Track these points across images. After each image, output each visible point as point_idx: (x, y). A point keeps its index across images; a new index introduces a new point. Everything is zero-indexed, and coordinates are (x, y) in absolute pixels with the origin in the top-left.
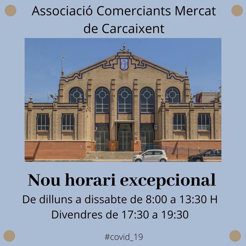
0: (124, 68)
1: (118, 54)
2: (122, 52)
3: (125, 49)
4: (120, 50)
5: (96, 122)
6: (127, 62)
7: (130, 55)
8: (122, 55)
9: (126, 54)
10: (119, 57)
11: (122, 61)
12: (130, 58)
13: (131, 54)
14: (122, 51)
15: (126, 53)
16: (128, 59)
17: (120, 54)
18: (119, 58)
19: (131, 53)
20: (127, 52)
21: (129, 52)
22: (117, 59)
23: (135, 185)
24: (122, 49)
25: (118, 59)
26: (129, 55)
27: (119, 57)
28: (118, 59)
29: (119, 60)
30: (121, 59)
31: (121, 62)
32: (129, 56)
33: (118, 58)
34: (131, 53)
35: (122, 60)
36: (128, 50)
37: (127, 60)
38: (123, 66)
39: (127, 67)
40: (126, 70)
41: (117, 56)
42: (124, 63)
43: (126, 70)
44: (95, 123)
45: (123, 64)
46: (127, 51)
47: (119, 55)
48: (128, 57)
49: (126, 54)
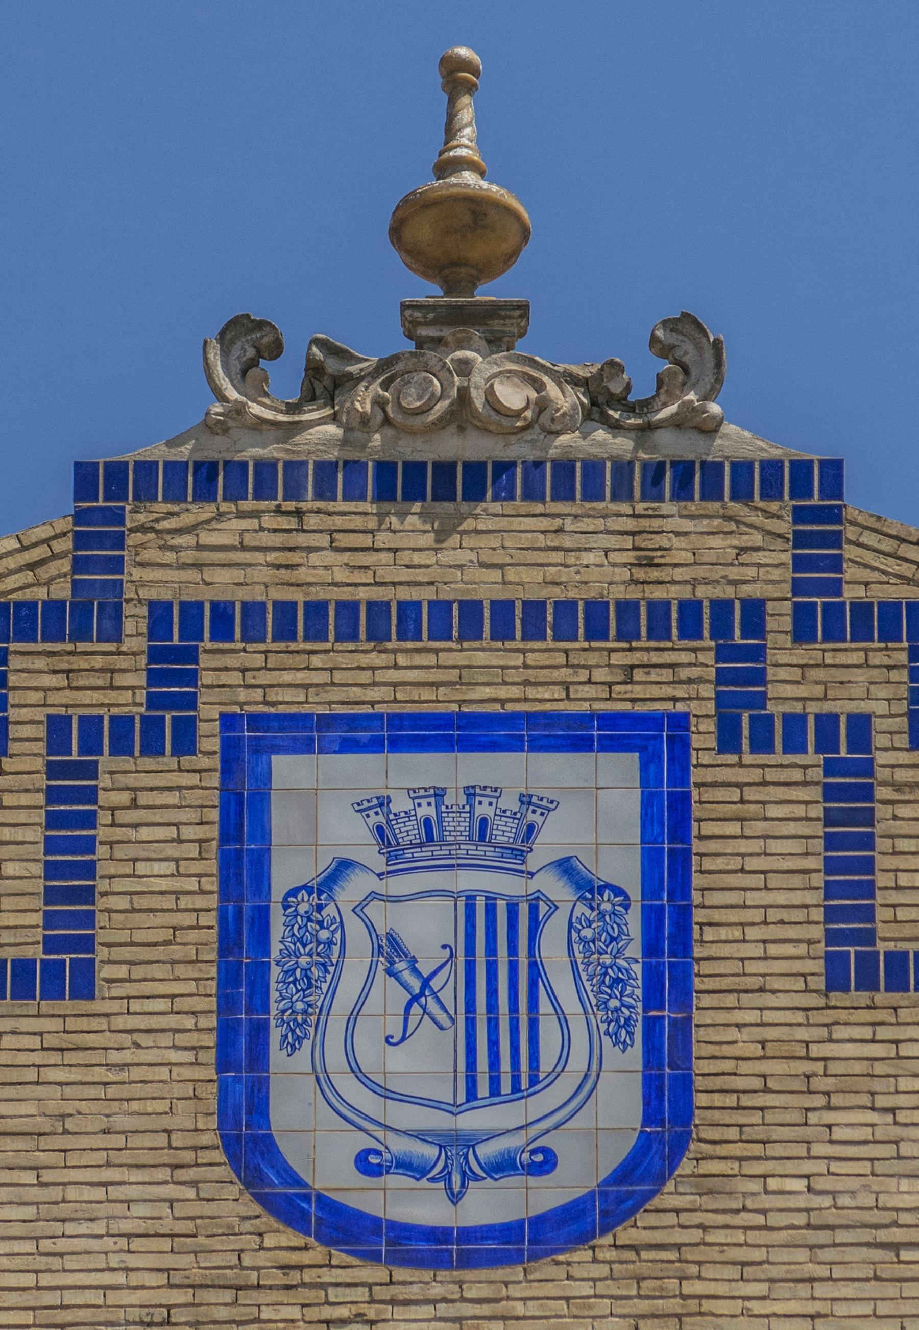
0: (456, 1162)
1: (98, 540)
2: (321, 434)
3: (500, 326)
4: (251, 341)
5: (908, 746)
6: (623, 867)
7: (783, 654)
8: (326, 574)
9: (586, 552)
10: (172, 670)
11: (349, 833)
12: (745, 718)
13: (819, 535)
14: (325, 383)
15: (572, 480)
16: (655, 740)
17: (226, 526)
18: (164, 726)
19: (812, 495)
20: (605, 443)
21: (737, 441)
22: (76, 749)
23: (568, 859)
24: (366, 299)
25: (117, 777)
26: (734, 554)
27: (172, 670)
28: (117, 777)
29: (155, 833)
30: (253, 740)
31: (287, 871)
32: (734, 630)
33: (129, 695)
34: (812, 495)
35: (322, 808)
36: (689, 347)
37: (594, 809)
38: (368, 1077)
39: (620, 1103)
40: (570, 1227)
41: (86, 615)
42: (428, 929)
43: (570, 1227)
44: (907, 750)
45: (391, 949)
46: (602, 400)
47: (185, 555)
48: (681, 680)
49: (586, 552)
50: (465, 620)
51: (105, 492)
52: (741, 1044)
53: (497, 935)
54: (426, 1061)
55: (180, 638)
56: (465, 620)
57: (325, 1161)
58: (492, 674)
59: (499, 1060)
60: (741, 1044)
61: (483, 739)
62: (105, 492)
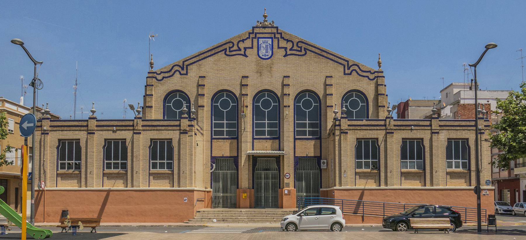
0: (265, 55)
1: (253, 30)
2: (261, 25)
3: (266, 21)
4: (258, 21)
7: (276, 31)
8: (261, 31)
9: (269, 30)
10: (256, 35)
12: (275, 37)
13: (277, 30)
14: (261, 23)
15: (269, 27)
16: (272, 38)
18: (255, 38)
19: (277, 28)
21: (275, 26)
22: (253, 38)
24: (262, 20)
26: (275, 31)
27: (256, 35)
29: (255, 41)
30: (259, 38)
33: (254, 36)
34: (277, 28)
35: (261, 41)
37: (270, 41)
38: (262, 52)
39: (271, 53)
41: (253, 33)
42: (264, 46)
44: (211, 156)
46: (270, 24)
47: (257, 30)
48: (273, 36)
49: (269, 30)
50: (266, 33)
51: (253, 28)
52: (380, 60)
53: (267, 46)
54: (264, 51)
55: (256, 33)
56: (266, 33)
57: (261, 55)
58: (267, 36)
59: (267, 52)
60: (380, 60)
61: (331, 146)
62: (253, 28)
